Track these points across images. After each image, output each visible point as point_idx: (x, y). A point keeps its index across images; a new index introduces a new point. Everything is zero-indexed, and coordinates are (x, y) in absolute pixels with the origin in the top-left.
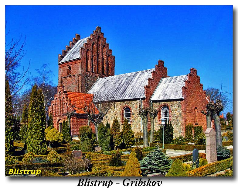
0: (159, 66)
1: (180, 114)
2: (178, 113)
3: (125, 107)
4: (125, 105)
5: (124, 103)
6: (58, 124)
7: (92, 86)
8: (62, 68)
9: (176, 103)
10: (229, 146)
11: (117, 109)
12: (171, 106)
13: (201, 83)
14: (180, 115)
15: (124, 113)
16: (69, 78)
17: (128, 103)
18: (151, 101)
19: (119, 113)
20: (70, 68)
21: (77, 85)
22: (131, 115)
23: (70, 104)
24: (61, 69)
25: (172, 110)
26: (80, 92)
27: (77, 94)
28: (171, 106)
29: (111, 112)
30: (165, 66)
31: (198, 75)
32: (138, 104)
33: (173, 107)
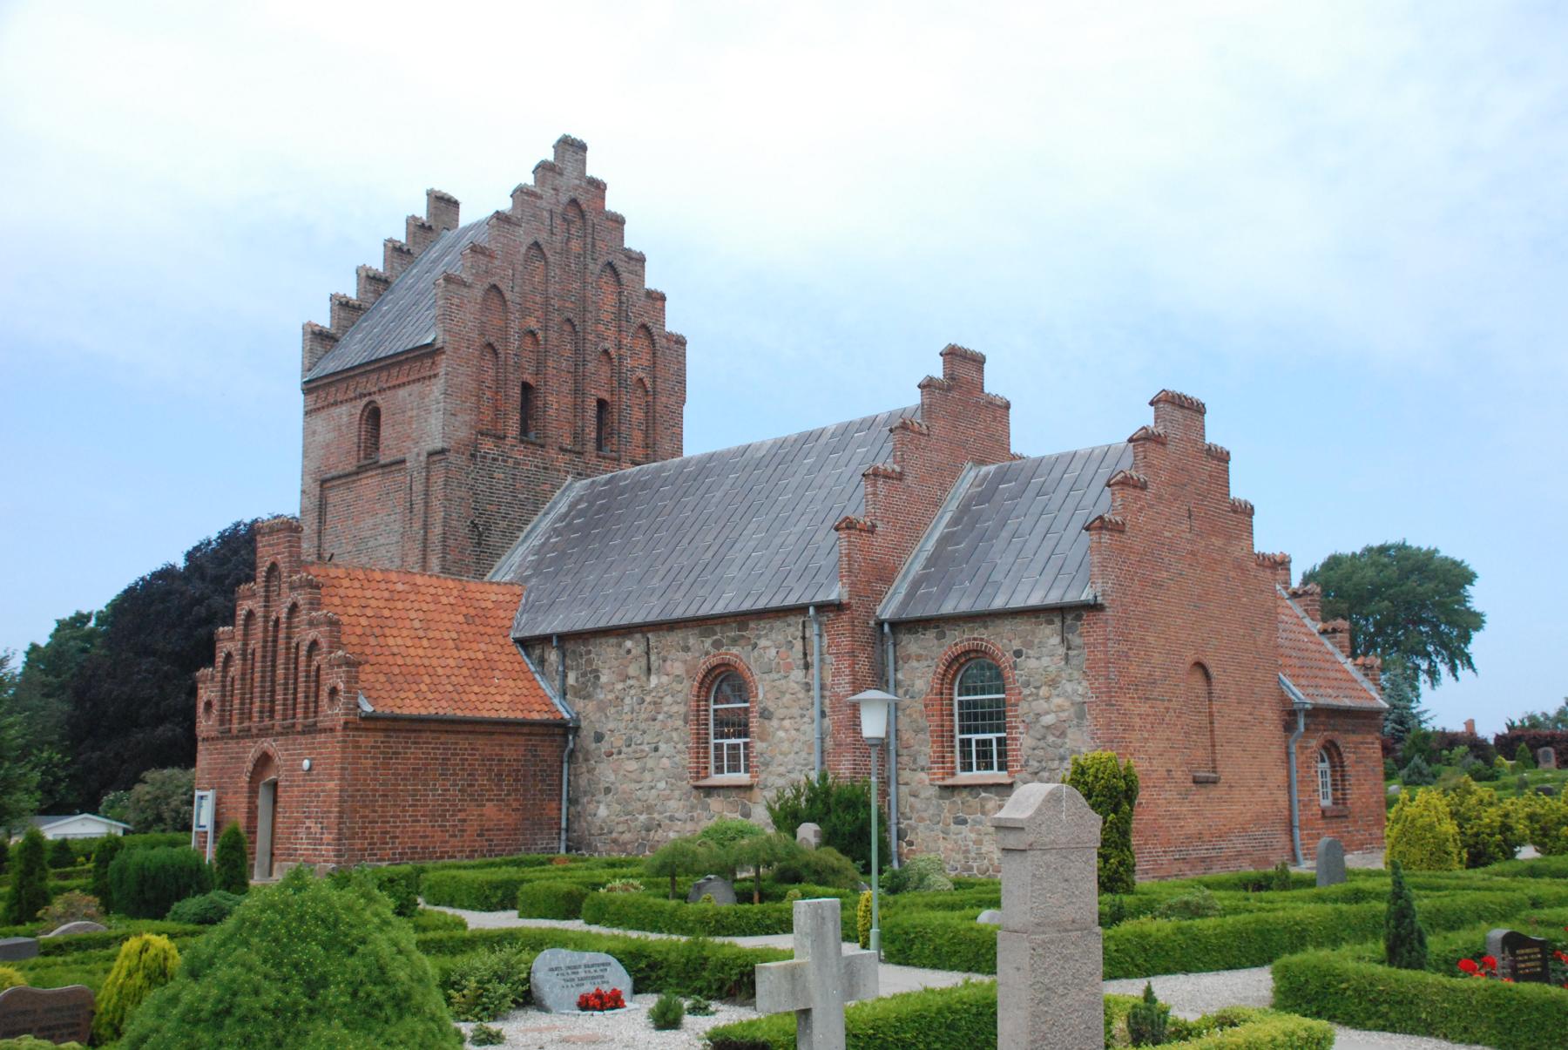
0: (950, 388)
1: (1081, 710)
2: (1067, 704)
3: (714, 668)
4: (713, 651)
5: (708, 642)
6: (253, 793)
7: (520, 529)
8: (323, 414)
9: (1049, 635)
10: (1124, 982)
11: (665, 679)
12: (1018, 654)
13: (1238, 491)
14: (1081, 716)
15: (957, 698)
16: (371, 483)
17: (734, 641)
18: (880, 624)
19: (675, 708)
20: (373, 416)
21: (417, 526)
22: (755, 724)
23: (336, 644)
24: (319, 422)
25: (1027, 684)
26: (437, 569)
27: (400, 587)
28: (1018, 654)
29: (628, 700)
30: (994, 383)
31: (1214, 435)
32: (798, 644)
33: (1032, 663)
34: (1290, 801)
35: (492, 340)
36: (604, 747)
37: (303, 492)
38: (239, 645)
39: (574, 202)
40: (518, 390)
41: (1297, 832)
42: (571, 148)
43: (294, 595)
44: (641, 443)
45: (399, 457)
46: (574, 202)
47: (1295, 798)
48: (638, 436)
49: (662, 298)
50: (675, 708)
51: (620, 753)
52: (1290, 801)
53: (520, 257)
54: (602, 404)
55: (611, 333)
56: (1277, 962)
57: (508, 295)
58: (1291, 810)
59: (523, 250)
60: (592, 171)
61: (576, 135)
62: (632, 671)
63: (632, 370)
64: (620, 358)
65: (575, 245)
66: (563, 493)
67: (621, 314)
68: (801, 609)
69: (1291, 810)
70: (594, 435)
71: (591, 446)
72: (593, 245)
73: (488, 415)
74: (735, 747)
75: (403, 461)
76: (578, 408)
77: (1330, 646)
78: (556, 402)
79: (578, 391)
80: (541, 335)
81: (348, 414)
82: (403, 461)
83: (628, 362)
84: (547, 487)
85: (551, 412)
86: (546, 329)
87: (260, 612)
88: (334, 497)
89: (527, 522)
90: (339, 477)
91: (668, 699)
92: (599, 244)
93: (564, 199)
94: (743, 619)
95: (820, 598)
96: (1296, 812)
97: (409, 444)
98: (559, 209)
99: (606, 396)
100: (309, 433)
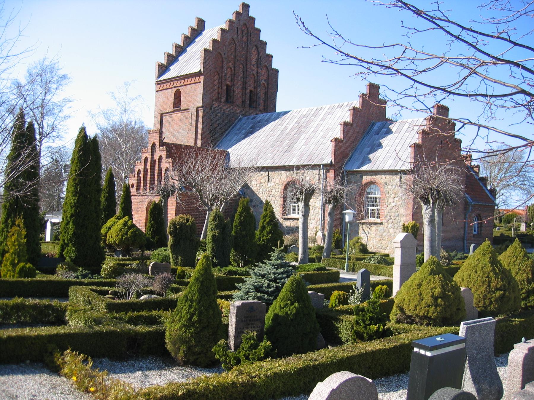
7: (225, 132)
19: (276, 193)
34: (464, 232)
35: (218, 70)
36: (253, 204)
37: (155, 117)
38: (143, 167)
39: (245, 24)
40: (225, 87)
41: (465, 241)
42: (246, 7)
43: (161, 153)
44: (263, 105)
45: (187, 108)
46: (245, 24)
47: (466, 231)
48: (262, 103)
49: (272, 57)
50: (276, 193)
51: (258, 206)
52: (464, 232)
53: (227, 43)
54: (251, 91)
55: (255, 69)
56: (460, 391)
57: (223, 56)
58: (464, 234)
59: (228, 40)
60: (251, 14)
61: (247, 2)
62: (263, 181)
63: (261, 81)
64: (257, 76)
65: (245, 39)
66: (238, 121)
67: (258, 64)
68: (319, 165)
69: (464, 234)
70: (248, 102)
71: (247, 106)
72: (250, 39)
73: (216, 95)
74: (295, 206)
75: (188, 109)
76: (244, 93)
77: (481, 185)
78: (237, 91)
79: (244, 87)
80: (233, 69)
81: (171, 93)
82: (188, 109)
83: (260, 78)
84: (233, 119)
85: (235, 94)
86: (235, 67)
87: (149, 158)
88: (165, 118)
89: (227, 130)
90: (167, 113)
91: (274, 191)
92: (252, 39)
93: (242, 24)
94: (298, 167)
95: (324, 163)
96: (466, 236)
97: (191, 104)
98: (240, 27)
99: (252, 89)
100: (157, 98)
